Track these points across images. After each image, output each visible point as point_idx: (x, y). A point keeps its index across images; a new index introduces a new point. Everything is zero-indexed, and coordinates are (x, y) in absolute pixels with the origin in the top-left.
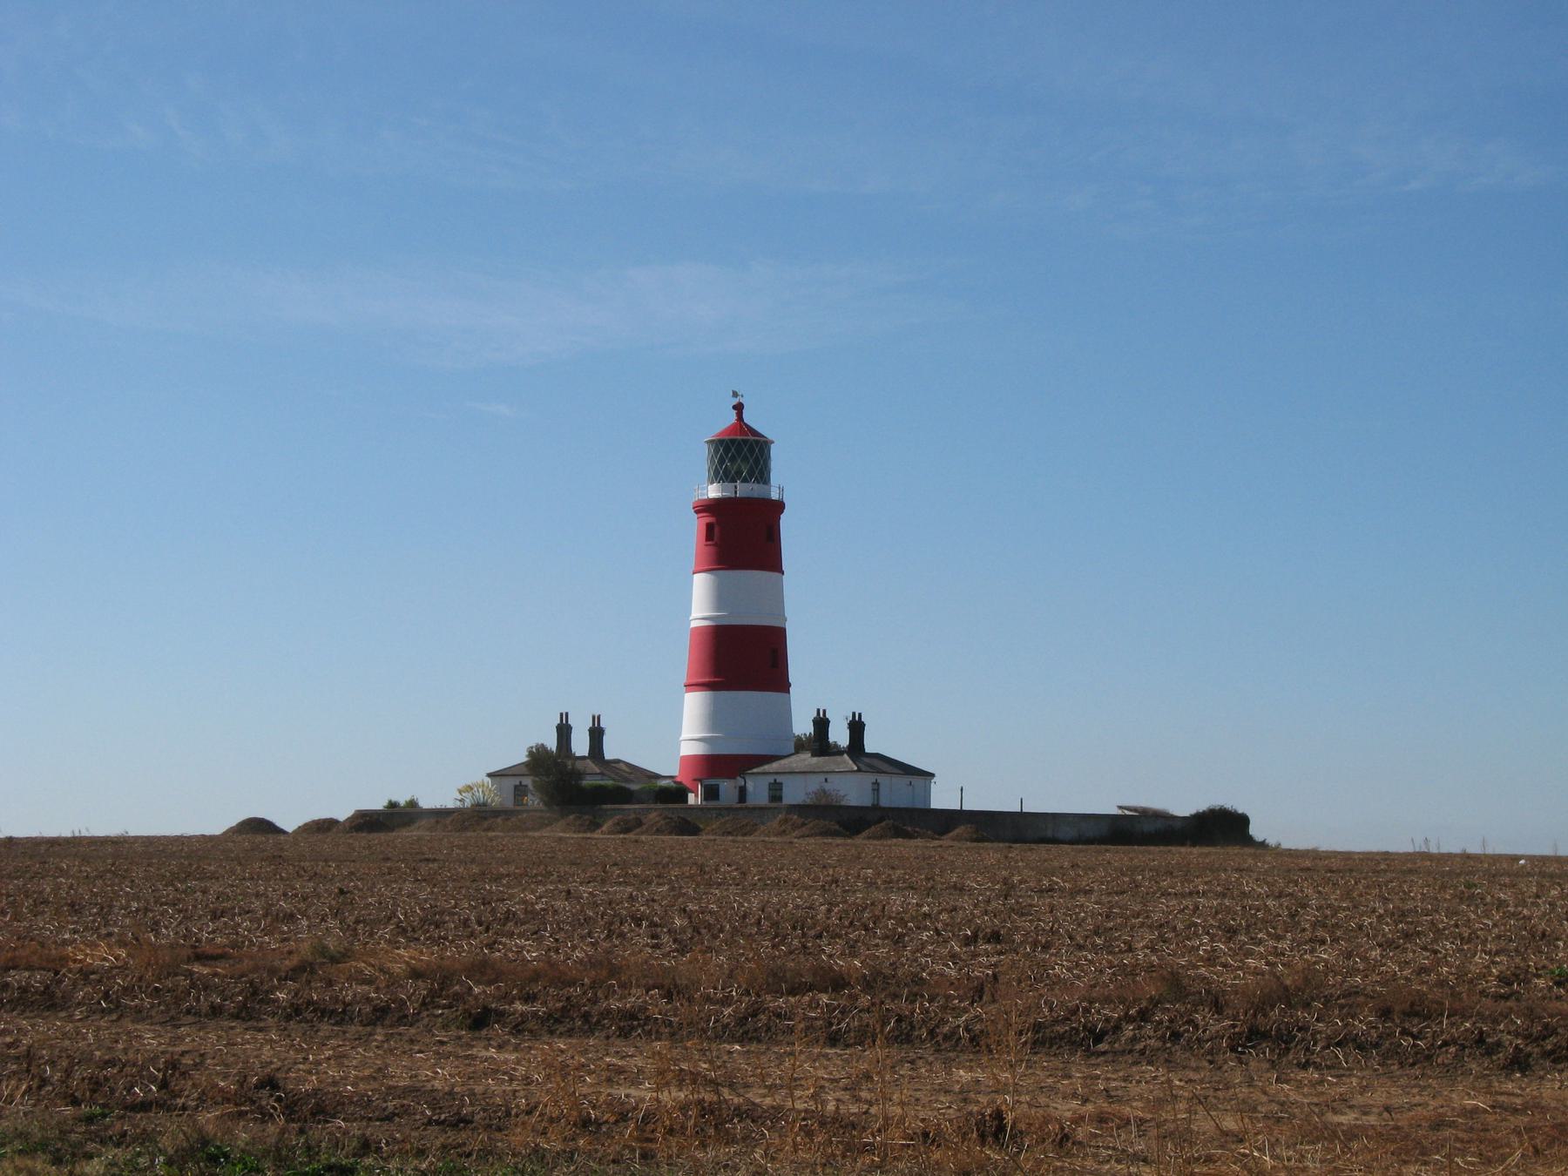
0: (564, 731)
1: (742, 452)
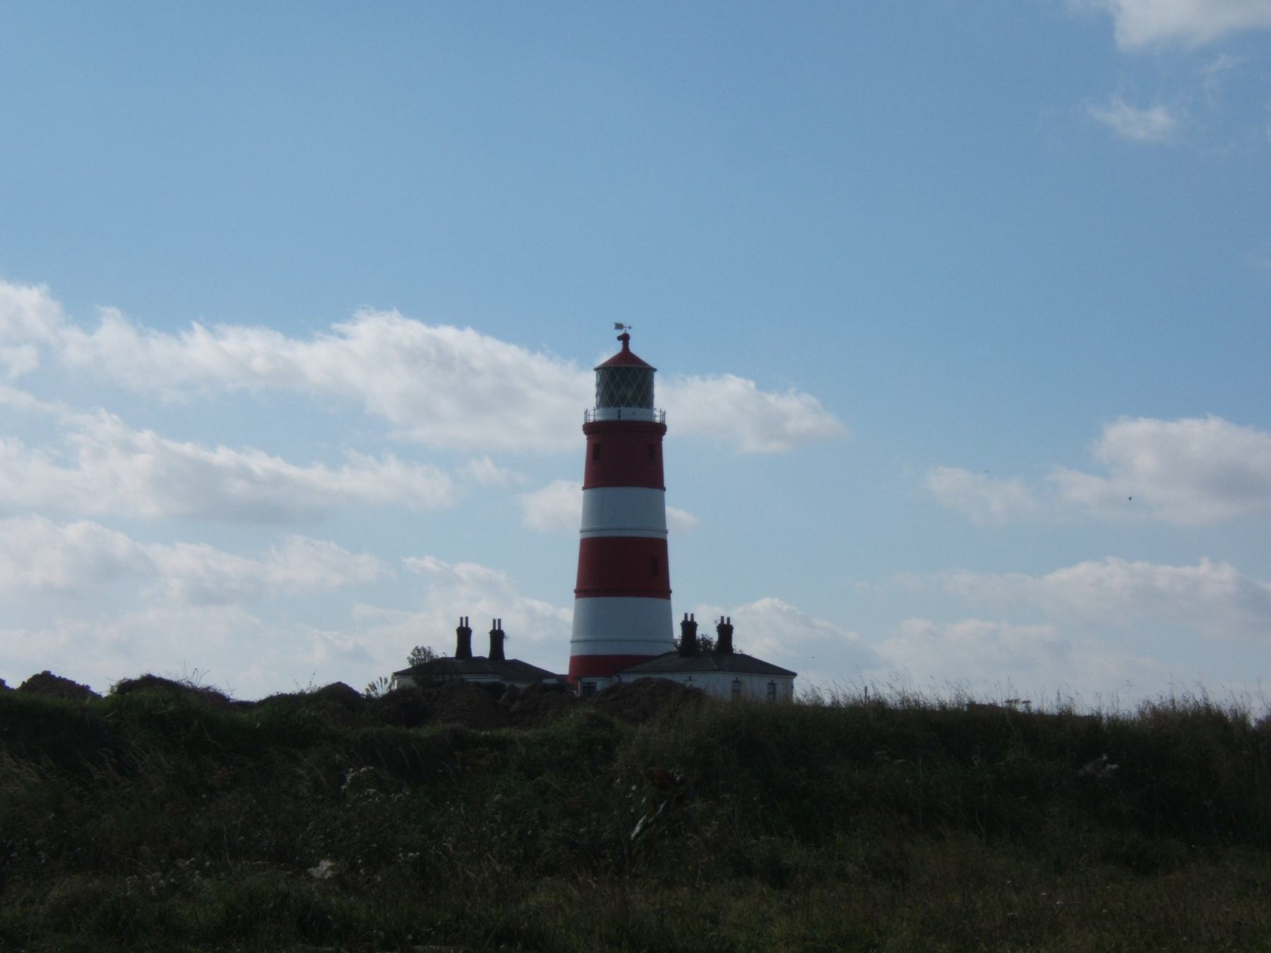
0: (464, 634)
1: (626, 379)
